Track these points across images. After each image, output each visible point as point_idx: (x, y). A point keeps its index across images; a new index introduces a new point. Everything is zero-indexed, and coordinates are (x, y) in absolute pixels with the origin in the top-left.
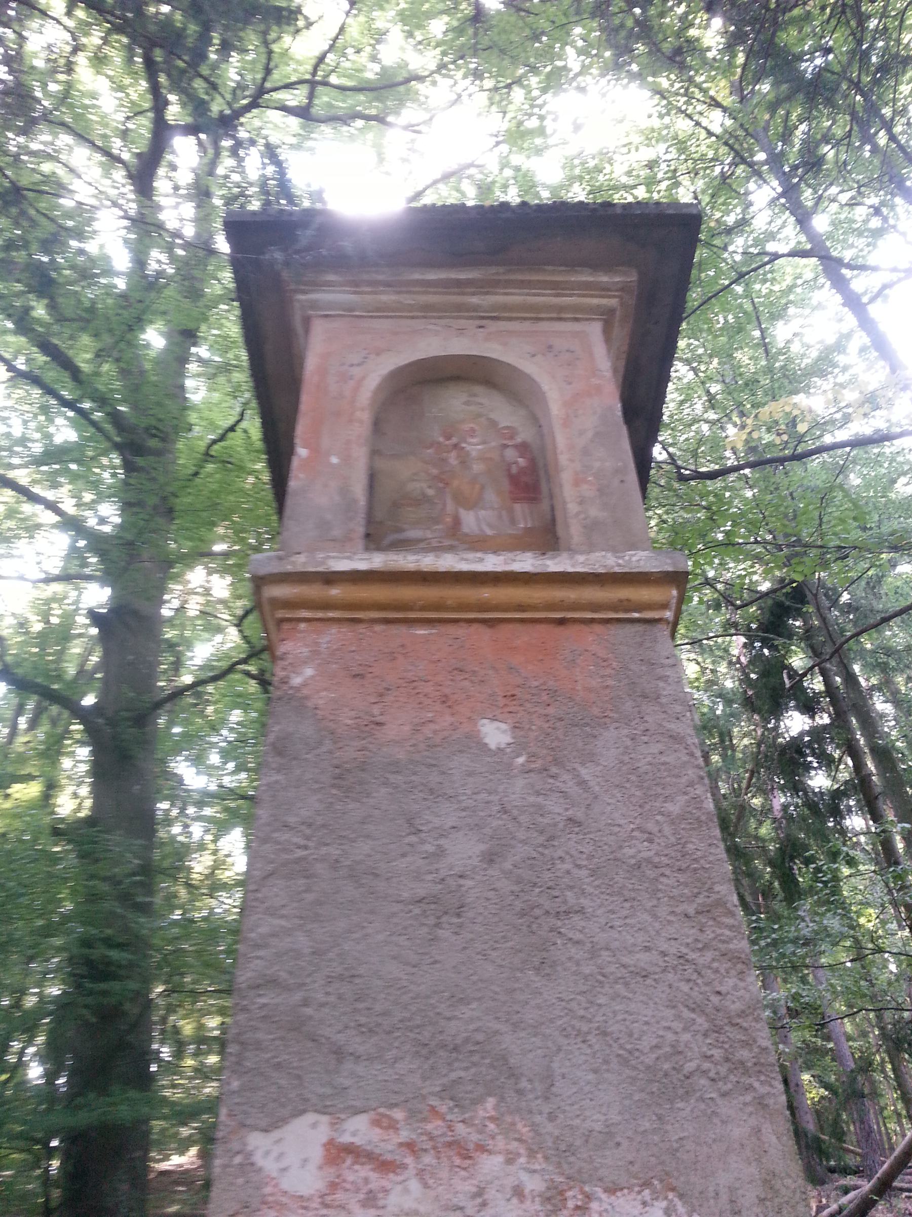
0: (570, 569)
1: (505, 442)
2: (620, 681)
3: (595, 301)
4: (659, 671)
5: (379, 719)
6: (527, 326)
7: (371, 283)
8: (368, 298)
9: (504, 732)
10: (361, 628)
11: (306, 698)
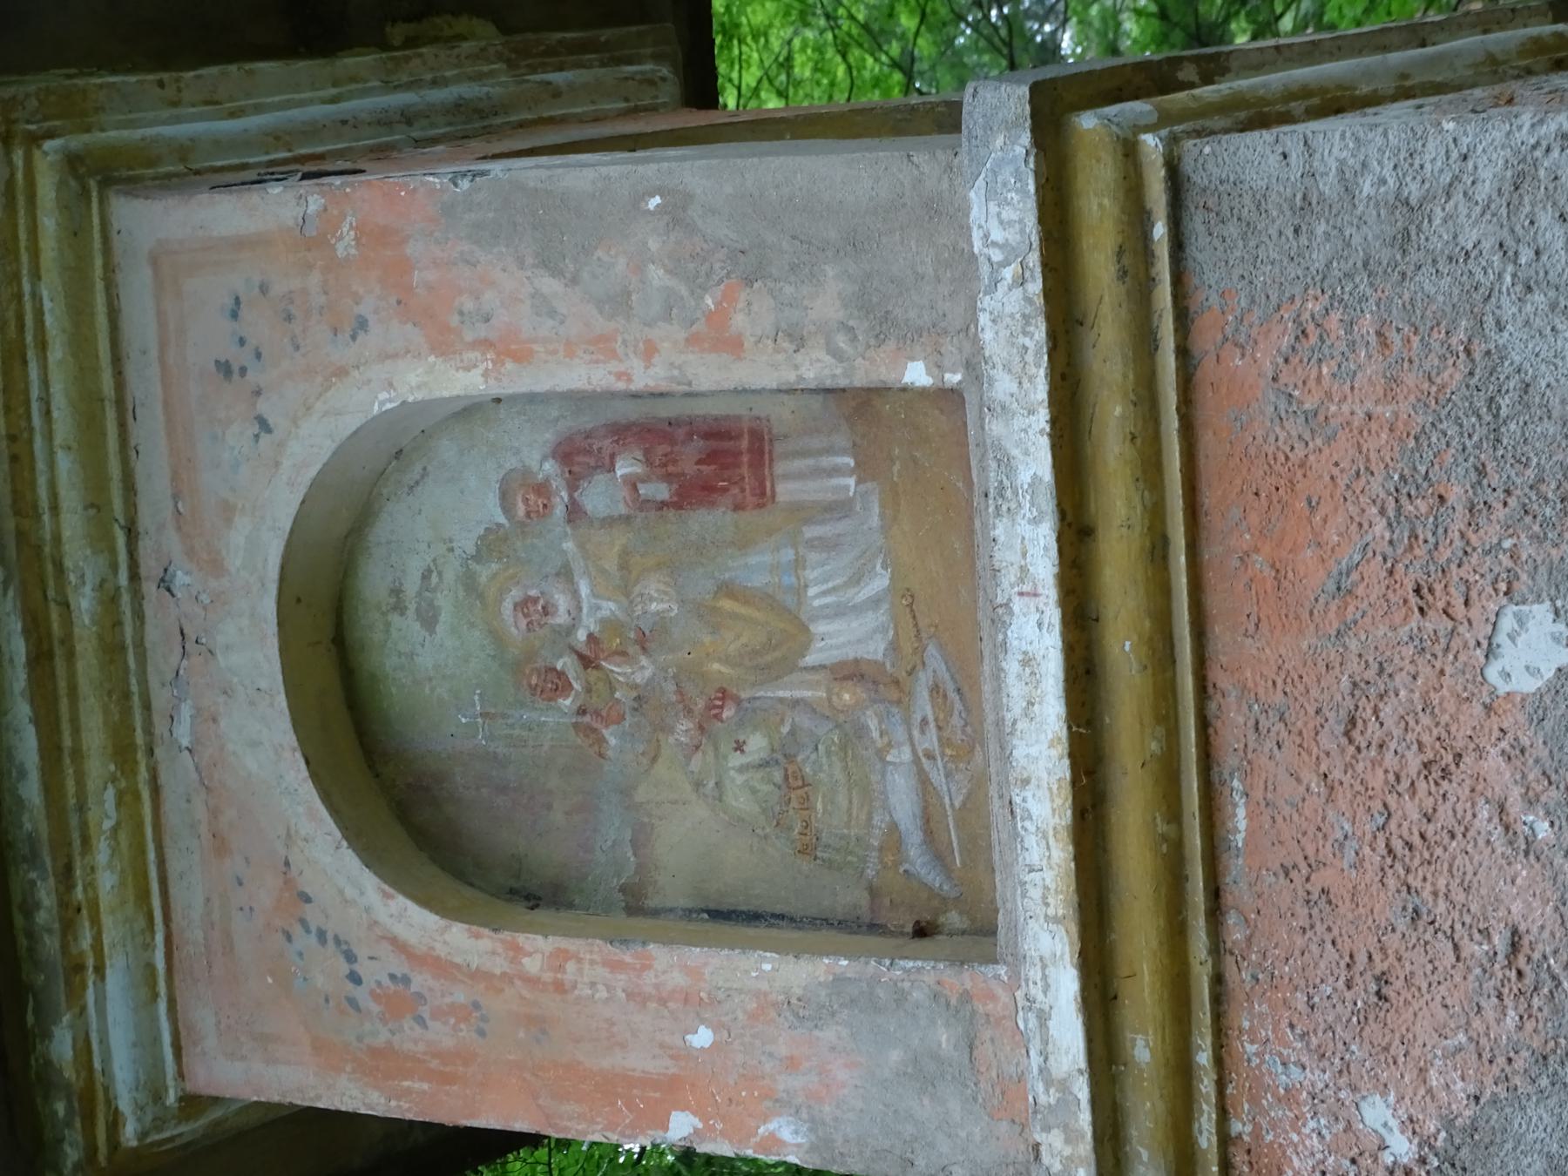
0: (1042, 418)
1: (559, 511)
2: (1364, 299)
3: (49, 224)
4: (1328, 186)
5: (1500, 941)
6: (150, 431)
7: (69, 915)
8: (112, 932)
9: (1521, 621)
10: (1239, 978)
11: (1449, 1123)
